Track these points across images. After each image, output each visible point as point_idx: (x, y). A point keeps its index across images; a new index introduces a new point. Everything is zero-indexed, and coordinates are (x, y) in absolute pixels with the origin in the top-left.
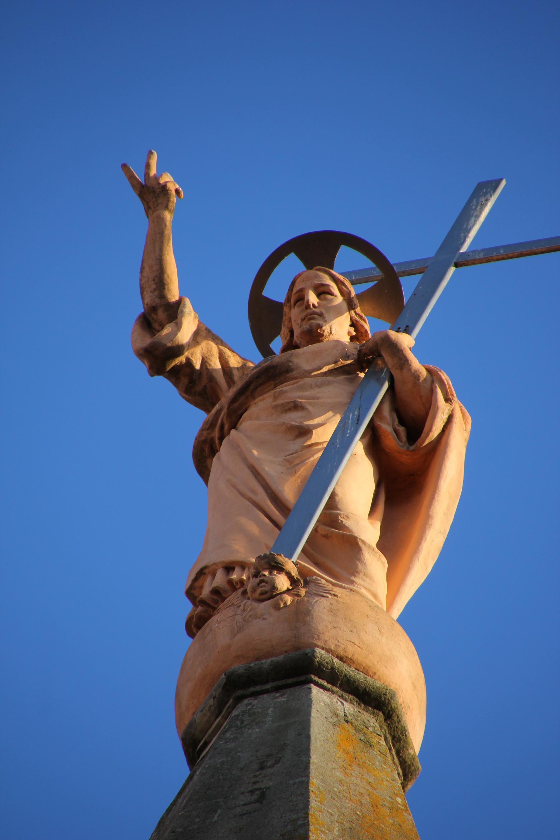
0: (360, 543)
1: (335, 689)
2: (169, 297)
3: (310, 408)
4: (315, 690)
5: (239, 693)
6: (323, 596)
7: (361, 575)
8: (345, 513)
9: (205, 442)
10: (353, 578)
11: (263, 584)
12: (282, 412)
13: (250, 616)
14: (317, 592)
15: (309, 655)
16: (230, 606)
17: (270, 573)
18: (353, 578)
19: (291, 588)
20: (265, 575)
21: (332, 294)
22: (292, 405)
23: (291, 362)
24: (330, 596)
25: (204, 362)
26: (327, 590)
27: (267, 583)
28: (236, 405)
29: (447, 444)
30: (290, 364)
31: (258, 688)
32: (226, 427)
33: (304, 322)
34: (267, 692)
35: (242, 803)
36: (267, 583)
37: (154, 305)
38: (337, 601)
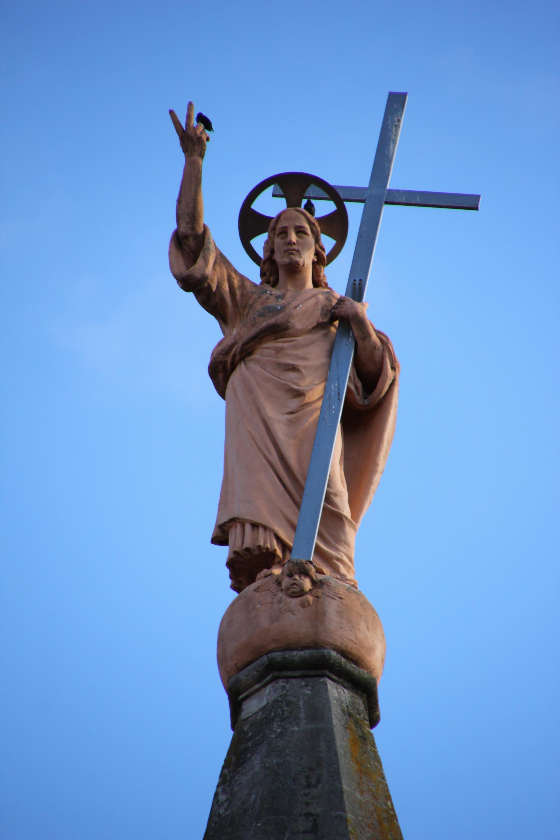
0: (344, 519)
1: (340, 680)
2: (198, 229)
3: (303, 371)
4: (330, 683)
5: (276, 674)
6: (333, 598)
7: (343, 543)
8: (335, 492)
9: (220, 362)
10: (338, 546)
11: (295, 586)
12: (283, 370)
13: (285, 609)
14: (328, 594)
15: (327, 657)
16: (267, 590)
17: (300, 577)
18: (338, 546)
19: (312, 588)
20: (296, 580)
21: (306, 233)
22: (291, 367)
23: (289, 322)
24: (337, 599)
25: (219, 286)
26: (335, 593)
27: (297, 585)
28: (247, 346)
29: (390, 403)
30: (289, 324)
31: (289, 673)
32: (237, 357)
33: (286, 254)
34: (295, 677)
35: (301, 828)
36: (297, 585)
37: (187, 234)
38: (342, 603)
